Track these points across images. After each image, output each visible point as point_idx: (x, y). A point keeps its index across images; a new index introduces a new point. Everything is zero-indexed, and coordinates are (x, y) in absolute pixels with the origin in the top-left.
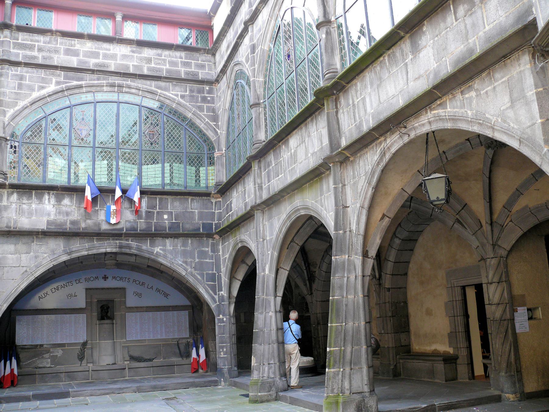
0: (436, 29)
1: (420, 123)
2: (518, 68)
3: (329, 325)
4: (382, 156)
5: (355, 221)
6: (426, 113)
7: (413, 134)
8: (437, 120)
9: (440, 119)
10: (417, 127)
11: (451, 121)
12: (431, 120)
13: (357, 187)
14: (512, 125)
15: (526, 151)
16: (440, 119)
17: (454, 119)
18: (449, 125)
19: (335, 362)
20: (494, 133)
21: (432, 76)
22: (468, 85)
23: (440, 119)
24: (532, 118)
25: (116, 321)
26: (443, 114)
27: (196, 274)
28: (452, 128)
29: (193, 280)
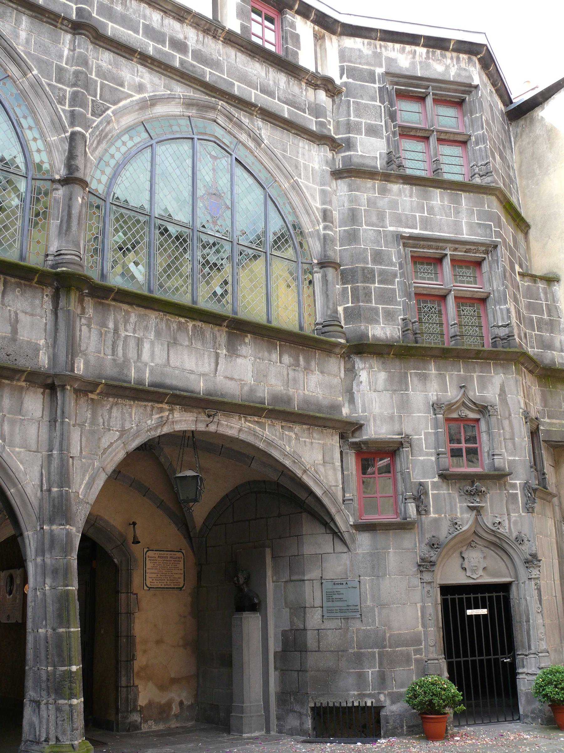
0: (259, 352)
1: (229, 424)
2: (331, 441)
3: (76, 629)
4: (159, 425)
5: (85, 482)
6: (240, 419)
7: (213, 428)
8: (250, 433)
9: (255, 435)
10: (223, 425)
11: (265, 443)
12: (244, 429)
13: (100, 439)
14: (322, 477)
15: (326, 501)
16: (255, 435)
17: (269, 443)
18: (261, 445)
19: (385, 734)
20: (303, 475)
21: (246, 389)
22: (289, 425)
23: (255, 435)
24: (337, 481)
25: (304, 458)
26: (260, 433)
27: (60, 110)
28: (263, 449)
29: (37, 103)
